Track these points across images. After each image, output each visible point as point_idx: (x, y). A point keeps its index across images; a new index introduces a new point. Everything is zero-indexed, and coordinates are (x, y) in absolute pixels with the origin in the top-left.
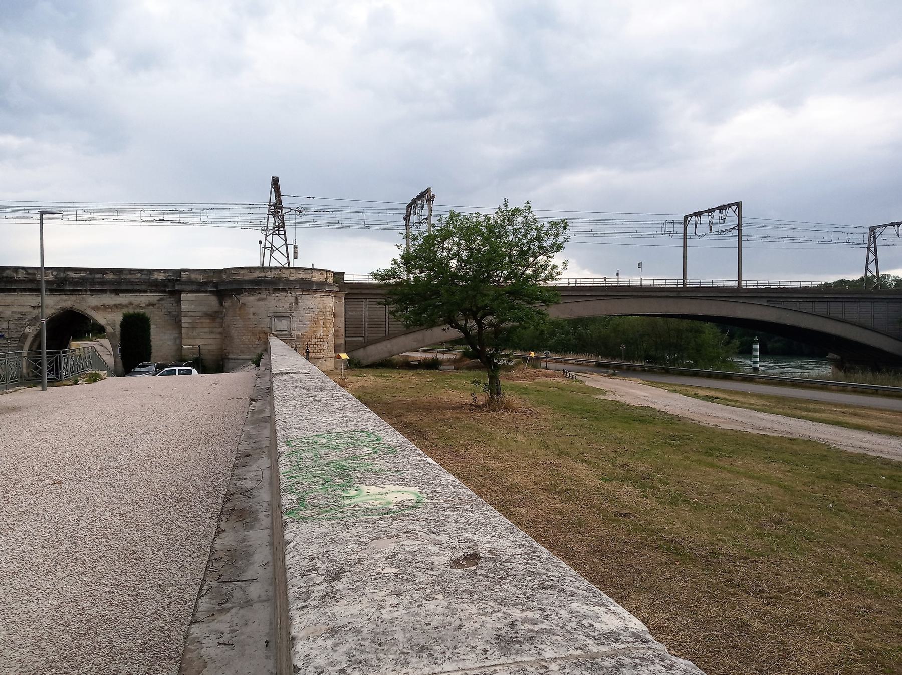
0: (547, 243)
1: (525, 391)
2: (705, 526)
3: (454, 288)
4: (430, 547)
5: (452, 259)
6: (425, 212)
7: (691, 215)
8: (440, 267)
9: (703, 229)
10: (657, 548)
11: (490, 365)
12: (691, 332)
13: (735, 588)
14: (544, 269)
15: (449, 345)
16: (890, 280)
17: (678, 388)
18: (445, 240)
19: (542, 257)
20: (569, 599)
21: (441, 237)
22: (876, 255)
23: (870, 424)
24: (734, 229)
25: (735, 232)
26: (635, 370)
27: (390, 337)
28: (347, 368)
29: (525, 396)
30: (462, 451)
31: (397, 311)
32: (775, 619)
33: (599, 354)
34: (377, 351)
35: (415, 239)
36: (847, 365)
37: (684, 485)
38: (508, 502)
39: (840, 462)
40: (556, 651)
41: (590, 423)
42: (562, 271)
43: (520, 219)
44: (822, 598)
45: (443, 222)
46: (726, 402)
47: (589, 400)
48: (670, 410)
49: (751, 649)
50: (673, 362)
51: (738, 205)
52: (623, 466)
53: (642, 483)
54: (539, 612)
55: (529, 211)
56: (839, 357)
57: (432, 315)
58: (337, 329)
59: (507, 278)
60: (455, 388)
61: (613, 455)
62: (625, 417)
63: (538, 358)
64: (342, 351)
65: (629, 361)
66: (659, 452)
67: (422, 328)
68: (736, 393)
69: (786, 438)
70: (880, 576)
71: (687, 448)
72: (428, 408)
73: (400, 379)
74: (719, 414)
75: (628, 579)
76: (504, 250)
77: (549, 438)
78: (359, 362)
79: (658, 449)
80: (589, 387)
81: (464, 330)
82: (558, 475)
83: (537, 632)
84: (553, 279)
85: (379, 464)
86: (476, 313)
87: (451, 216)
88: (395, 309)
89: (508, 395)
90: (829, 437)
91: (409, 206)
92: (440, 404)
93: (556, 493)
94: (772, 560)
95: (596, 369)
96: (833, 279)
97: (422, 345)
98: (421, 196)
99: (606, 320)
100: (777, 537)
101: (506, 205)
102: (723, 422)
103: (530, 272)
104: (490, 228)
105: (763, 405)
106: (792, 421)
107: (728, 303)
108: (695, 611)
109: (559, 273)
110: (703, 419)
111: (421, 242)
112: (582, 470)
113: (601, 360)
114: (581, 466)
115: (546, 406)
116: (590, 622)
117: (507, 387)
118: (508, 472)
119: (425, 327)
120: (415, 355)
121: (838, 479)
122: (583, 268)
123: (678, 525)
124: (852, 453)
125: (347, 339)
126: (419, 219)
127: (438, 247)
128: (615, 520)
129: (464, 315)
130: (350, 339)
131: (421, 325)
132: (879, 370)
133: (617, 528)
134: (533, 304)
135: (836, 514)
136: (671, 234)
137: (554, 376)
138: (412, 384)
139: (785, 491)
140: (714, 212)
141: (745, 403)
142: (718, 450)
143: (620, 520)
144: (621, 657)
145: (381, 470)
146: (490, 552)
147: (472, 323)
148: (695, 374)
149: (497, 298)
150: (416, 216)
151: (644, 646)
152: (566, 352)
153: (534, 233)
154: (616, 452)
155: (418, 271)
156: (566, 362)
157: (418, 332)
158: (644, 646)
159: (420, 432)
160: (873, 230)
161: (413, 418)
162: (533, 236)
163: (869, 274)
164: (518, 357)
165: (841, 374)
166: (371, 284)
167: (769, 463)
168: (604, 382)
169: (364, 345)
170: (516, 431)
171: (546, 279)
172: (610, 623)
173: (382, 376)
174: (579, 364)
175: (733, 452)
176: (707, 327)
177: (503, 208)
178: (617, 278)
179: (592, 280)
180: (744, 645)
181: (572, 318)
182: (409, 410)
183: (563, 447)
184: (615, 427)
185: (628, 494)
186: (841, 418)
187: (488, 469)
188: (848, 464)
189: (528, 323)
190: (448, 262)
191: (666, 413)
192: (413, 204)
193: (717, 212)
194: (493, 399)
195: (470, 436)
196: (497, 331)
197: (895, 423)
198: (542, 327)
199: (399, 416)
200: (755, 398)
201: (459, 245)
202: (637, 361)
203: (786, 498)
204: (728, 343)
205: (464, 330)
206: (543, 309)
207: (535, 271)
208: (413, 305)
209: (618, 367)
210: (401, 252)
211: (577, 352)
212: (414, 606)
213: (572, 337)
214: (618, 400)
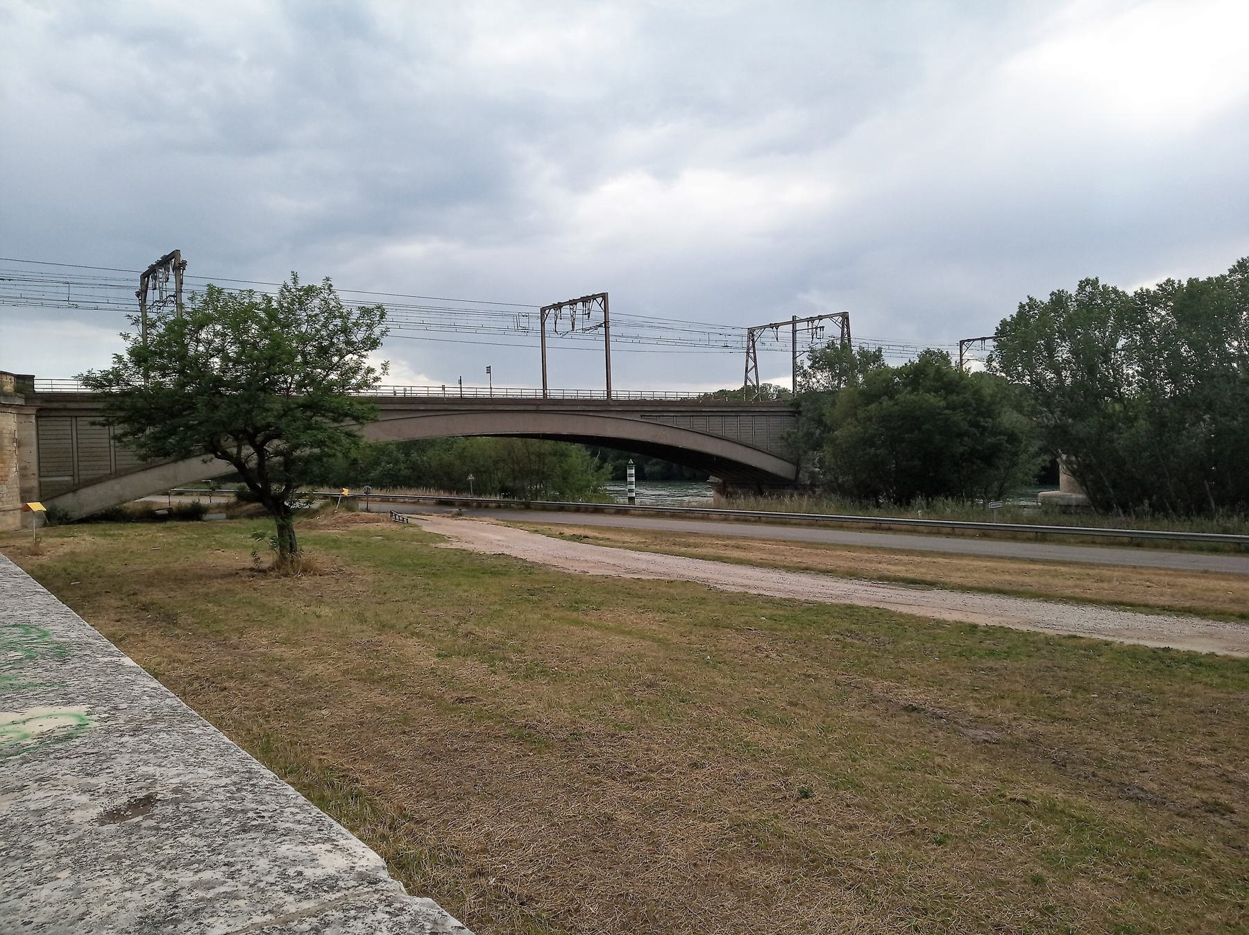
0: (358, 336)
1: (336, 544)
2: (565, 701)
3: (217, 399)
4: (74, 797)
5: (213, 356)
6: (172, 285)
7: (550, 308)
8: (191, 368)
9: (564, 325)
10: (506, 738)
11: (277, 509)
12: (555, 455)
13: (599, 774)
14: (355, 372)
15: (213, 484)
16: (772, 390)
17: (540, 528)
18: (201, 327)
19: (350, 356)
20: (279, 840)
21: (194, 323)
22: (755, 362)
23: (752, 558)
24: (600, 326)
25: (602, 330)
26: (487, 507)
27: (118, 474)
28: (45, 525)
29: (334, 551)
30: (234, 639)
31: (125, 435)
32: (645, 805)
33: (441, 487)
34: (95, 498)
35: (153, 325)
36: (730, 489)
37: (543, 651)
38: (305, 704)
39: (720, 605)
40: (231, 922)
41: (426, 581)
42: (381, 376)
43: (317, 302)
44: (697, 771)
45: (197, 302)
46: (596, 541)
47: (426, 551)
48: (530, 557)
49: (616, 849)
50: (536, 494)
51: (604, 296)
52: (466, 635)
53: (490, 654)
54: (224, 868)
55: (330, 290)
56: (721, 481)
57: (183, 439)
58: (23, 464)
59: (300, 385)
60: (227, 546)
61: (454, 622)
62: (473, 570)
63: (354, 498)
64: (35, 499)
65: (480, 495)
66: (513, 611)
67: (167, 460)
68: (609, 529)
69: (663, 580)
70: (758, 735)
71: (549, 604)
72: (180, 579)
73: (138, 538)
74: (589, 558)
75: (468, 785)
76: (295, 345)
77: (367, 608)
78: (66, 515)
79: (513, 608)
80: (426, 534)
81: (237, 462)
82: (378, 658)
83: (210, 900)
84: (369, 386)
85: (29, 675)
86: (255, 436)
87: (210, 294)
88: (121, 431)
89: (308, 551)
90: (709, 575)
91: (145, 276)
92: (203, 572)
93: (373, 682)
94: (643, 732)
95: (437, 508)
96: (713, 389)
97: (172, 485)
98: (164, 262)
99: (449, 442)
100: (649, 704)
101: (295, 281)
102: (592, 567)
103: (333, 376)
104: (272, 314)
105: (638, 543)
106: (671, 561)
107: (597, 419)
108: (550, 812)
109: (376, 379)
110: (567, 564)
111: (161, 331)
112: (412, 646)
113: (444, 495)
114: (410, 642)
115: (365, 563)
116: (299, 868)
117: (309, 540)
118: (306, 662)
119: (172, 458)
120: (164, 500)
121: (717, 625)
122: (418, 373)
123: (533, 703)
124: (732, 593)
125: (42, 479)
126: (161, 296)
127: (191, 339)
128: (454, 709)
129: (236, 438)
130: (48, 479)
131: (167, 454)
132: (761, 493)
133: (456, 719)
134: (342, 421)
135: (714, 667)
136: (525, 330)
137: (378, 521)
138: (157, 544)
139: (660, 645)
140: (576, 304)
141: (618, 541)
142: (585, 602)
143: (460, 708)
144: (329, 913)
145: (30, 684)
146: (175, 791)
147: (248, 450)
148: (561, 509)
149: (285, 414)
150: (157, 292)
151: (371, 889)
152: (395, 487)
153: (338, 322)
154: (459, 618)
155: (157, 374)
156: (395, 500)
157: (167, 466)
158: (371, 889)
159: (168, 616)
160: (751, 332)
161: (156, 595)
162: (336, 325)
163: (749, 383)
164: (325, 497)
165: (723, 500)
166: (83, 394)
167: (643, 613)
168: (447, 525)
169: (74, 489)
170: (320, 601)
171: (358, 387)
172: (331, 863)
173: (105, 535)
174: (414, 503)
175: (602, 603)
176: (574, 447)
177: (290, 284)
178: (459, 386)
179: (426, 389)
180: (609, 844)
181: (401, 440)
182: (150, 584)
183: (386, 617)
184: (458, 585)
185: (470, 671)
186: (722, 553)
187: (274, 660)
188: (727, 606)
189: (333, 448)
190: (207, 361)
191: (525, 561)
192: (151, 272)
193: (580, 305)
194: (285, 558)
195: (248, 615)
196: (289, 462)
197: (776, 554)
198: (354, 454)
199: (135, 594)
200: (629, 534)
201: (224, 335)
202: (491, 495)
203: (660, 654)
204: (599, 468)
205: (237, 462)
206: (355, 428)
207: (342, 375)
208: (154, 425)
209: (466, 504)
210: (129, 344)
211: (410, 487)
212: (12, 897)
213: (402, 466)
214: (463, 548)
